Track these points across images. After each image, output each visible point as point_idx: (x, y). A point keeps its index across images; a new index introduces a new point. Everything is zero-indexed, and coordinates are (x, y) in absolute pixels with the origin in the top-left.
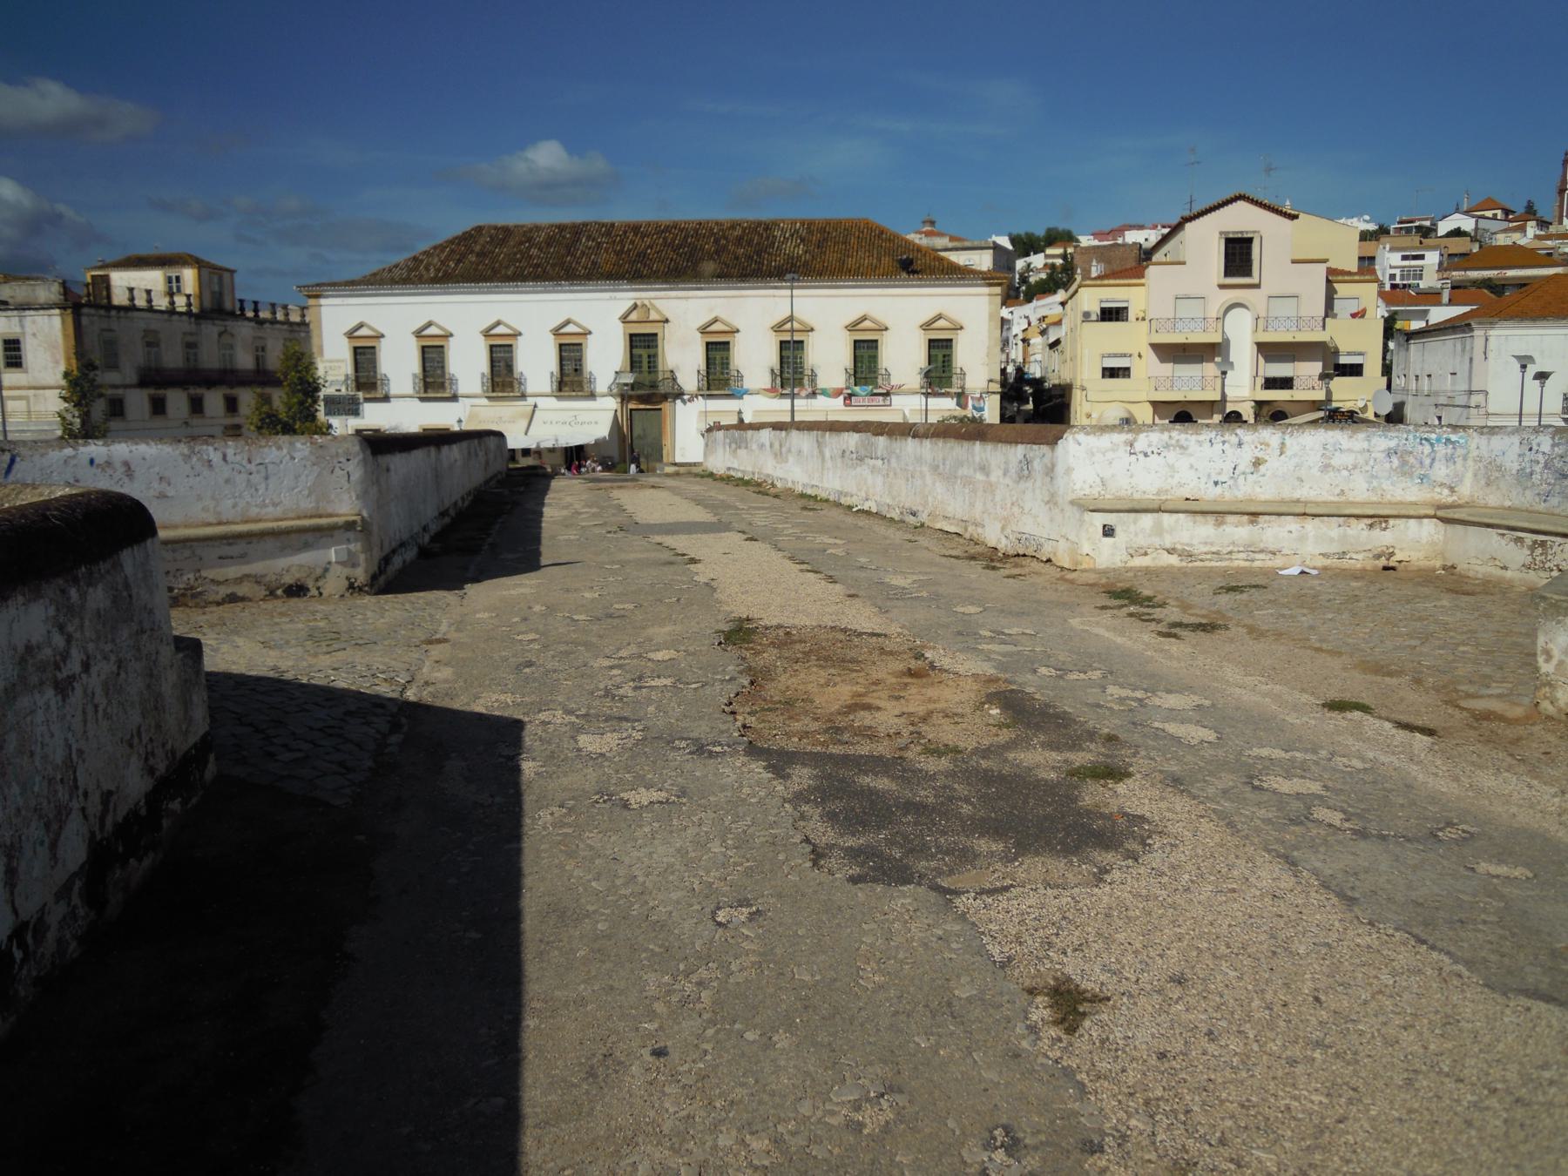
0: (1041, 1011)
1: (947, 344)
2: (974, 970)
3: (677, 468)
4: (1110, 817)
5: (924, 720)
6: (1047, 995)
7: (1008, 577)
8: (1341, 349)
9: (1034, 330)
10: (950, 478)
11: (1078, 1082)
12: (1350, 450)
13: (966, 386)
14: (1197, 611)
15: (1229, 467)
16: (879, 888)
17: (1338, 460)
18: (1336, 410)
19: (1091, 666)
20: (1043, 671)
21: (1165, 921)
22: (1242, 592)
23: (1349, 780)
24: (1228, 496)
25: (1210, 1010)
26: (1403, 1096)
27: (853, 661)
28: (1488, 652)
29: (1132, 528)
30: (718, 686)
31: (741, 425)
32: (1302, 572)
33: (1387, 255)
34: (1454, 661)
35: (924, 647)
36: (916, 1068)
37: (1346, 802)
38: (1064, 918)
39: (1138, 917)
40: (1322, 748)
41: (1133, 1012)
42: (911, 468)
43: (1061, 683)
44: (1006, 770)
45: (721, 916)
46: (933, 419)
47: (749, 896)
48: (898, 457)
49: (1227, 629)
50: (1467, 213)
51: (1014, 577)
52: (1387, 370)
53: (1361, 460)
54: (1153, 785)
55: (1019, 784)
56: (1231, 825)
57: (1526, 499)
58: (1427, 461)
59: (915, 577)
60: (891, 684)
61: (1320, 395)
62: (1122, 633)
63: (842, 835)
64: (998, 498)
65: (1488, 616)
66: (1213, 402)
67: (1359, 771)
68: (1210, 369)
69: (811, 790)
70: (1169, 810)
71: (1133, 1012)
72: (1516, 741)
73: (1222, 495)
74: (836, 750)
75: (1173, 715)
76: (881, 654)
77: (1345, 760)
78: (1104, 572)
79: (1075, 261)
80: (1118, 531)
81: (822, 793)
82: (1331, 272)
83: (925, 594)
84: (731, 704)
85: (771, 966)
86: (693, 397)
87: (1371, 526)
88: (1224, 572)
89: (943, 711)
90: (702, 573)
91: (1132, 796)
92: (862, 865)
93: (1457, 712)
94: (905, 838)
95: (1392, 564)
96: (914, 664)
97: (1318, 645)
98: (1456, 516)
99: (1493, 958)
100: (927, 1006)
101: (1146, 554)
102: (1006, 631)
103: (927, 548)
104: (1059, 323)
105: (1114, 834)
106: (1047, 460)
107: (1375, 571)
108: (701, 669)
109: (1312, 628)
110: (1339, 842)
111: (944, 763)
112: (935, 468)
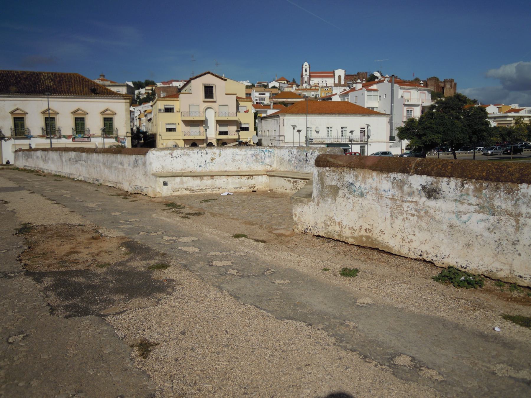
0: (135, 352)
1: (111, 119)
2: (111, 342)
3: (2, 166)
4: (162, 281)
5: (97, 255)
6: (138, 346)
7: (131, 201)
8: (242, 122)
9: (142, 115)
10: (110, 167)
11: (147, 375)
12: (240, 155)
13: (119, 134)
14: (195, 209)
15: (204, 161)
16: (77, 319)
17: (237, 158)
18: (241, 142)
19: (158, 230)
20: (142, 233)
21: (179, 314)
22: (209, 201)
23: (239, 259)
24: (204, 170)
25: (193, 341)
26: (251, 357)
27: (71, 236)
28: (281, 215)
29: (173, 182)
30: (14, 251)
31: (30, 149)
32: (228, 194)
33: (255, 93)
34: (271, 219)
35: (98, 228)
36: (88, 382)
37: (238, 267)
38: (145, 318)
39: (170, 314)
40: (232, 250)
41: (167, 347)
42: (95, 164)
43: (148, 237)
44: (127, 269)
45: (11, 340)
46: (107, 146)
47: (23, 330)
48: (91, 160)
49: (204, 214)
50: (277, 81)
51: (133, 201)
52: (256, 129)
53: (244, 158)
54: (177, 269)
55: (132, 274)
56: (202, 279)
57: (291, 168)
58: (263, 158)
59: (97, 203)
60: (86, 243)
61: (236, 137)
62: (170, 218)
63: (63, 301)
64: (127, 174)
65: (281, 204)
66: (203, 140)
67: (243, 256)
68: (202, 129)
69: (52, 286)
70: (182, 276)
71: (167, 347)
72: (288, 242)
73: (202, 170)
74: (62, 269)
75: (186, 244)
76: (82, 232)
77: (238, 253)
78: (165, 198)
79: (156, 92)
80: (169, 183)
81: (55, 287)
82: (238, 98)
83: (100, 209)
84: (20, 256)
85: (32, 355)
86: (9, 139)
87: (248, 178)
88: (204, 195)
89: (105, 251)
90: (10, 207)
91: (170, 273)
92: (70, 311)
93: (272, 234)
94: (88, 298)
95: (255, 190)
96: (95, 235)
97: (232, 217)
98: (272, 174)
99: (278, 309)
100: (93, 359)
101: (178, 191)
102: (129, 220)
103: (102, 193)
104: (151, 113)
105: (163, 287)
106: (143, 160)
107: (250, 192)
108: (7, 244)
109: (230, 212)
110: (235, 280)
111: (104, 269)
112: (104, 164)
